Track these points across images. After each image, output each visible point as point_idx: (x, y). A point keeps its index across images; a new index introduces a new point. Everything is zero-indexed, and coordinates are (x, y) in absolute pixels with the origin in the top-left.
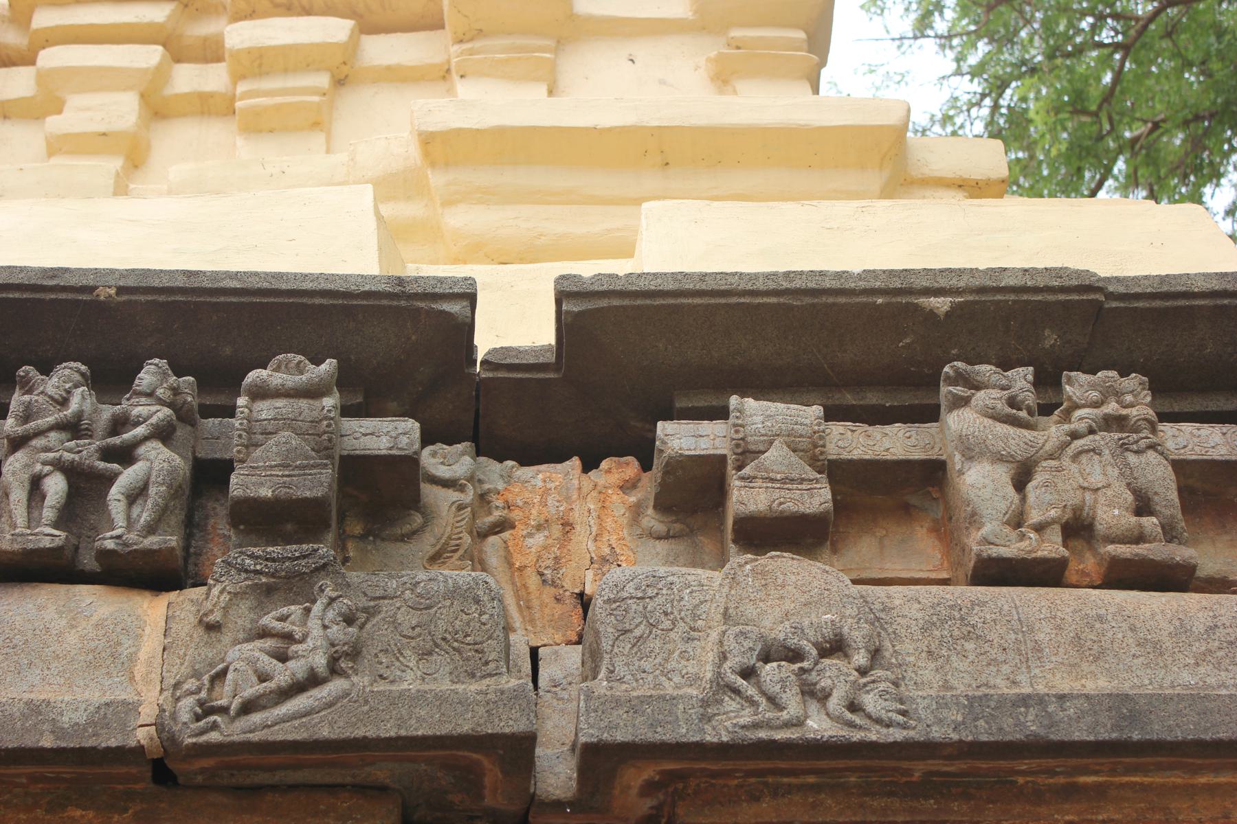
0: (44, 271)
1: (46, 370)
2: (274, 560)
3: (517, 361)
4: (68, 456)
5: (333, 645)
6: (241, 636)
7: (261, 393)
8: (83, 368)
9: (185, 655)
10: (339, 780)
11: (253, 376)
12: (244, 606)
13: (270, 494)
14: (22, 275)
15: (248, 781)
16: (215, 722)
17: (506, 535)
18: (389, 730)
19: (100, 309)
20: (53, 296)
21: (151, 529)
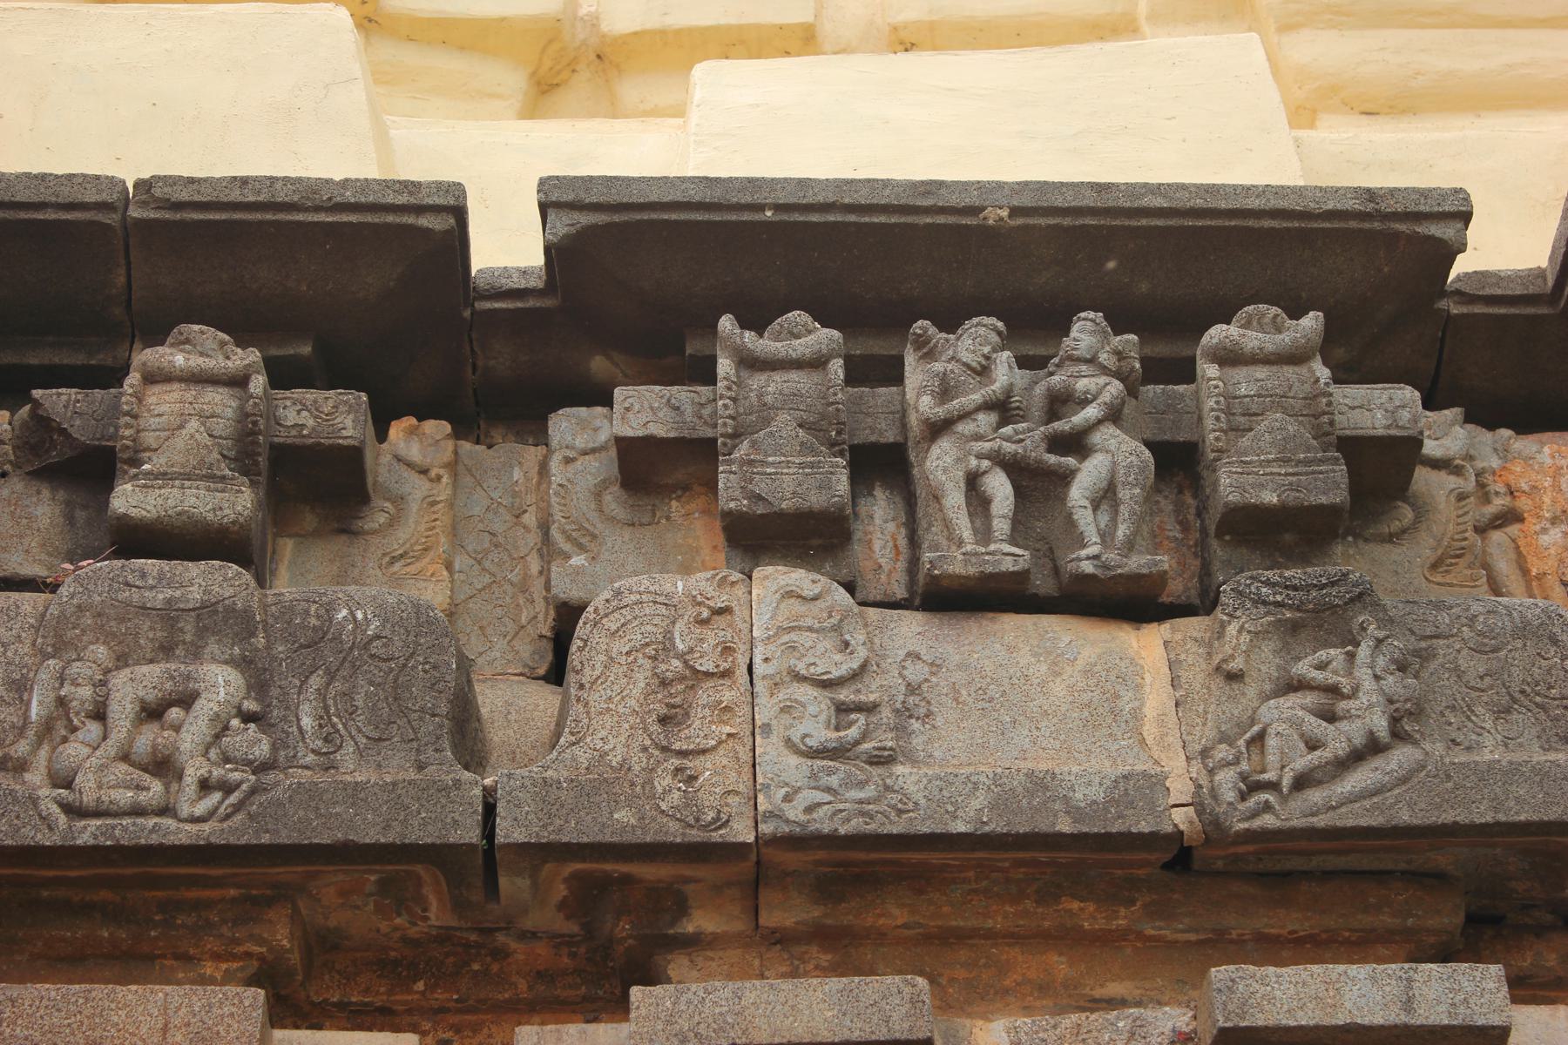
0: (914, 185)
1: (950, 323)
2: (1295, 588)
3: (1499, 292)
4: (1009, 447)
5: (1391, 701)
6: (1268, 687)
7: (1229, 358)
8: (1000, 324)
9: (1206, 713)
10: (1390, 866)
11: (1216, 334)
12: (1267, 649)
13: (1275, 500)
14: (887, 192)
15: (1278, 867)
16: (1267, 801)
17: (1514, 529)
18: (1483, 814)
19: (990, 235)
20: (929, 220)
21: (1130, 546)
